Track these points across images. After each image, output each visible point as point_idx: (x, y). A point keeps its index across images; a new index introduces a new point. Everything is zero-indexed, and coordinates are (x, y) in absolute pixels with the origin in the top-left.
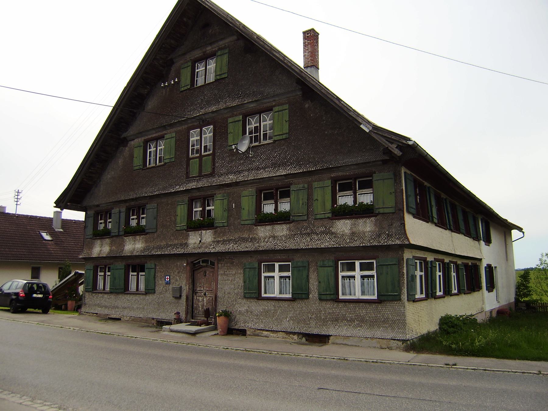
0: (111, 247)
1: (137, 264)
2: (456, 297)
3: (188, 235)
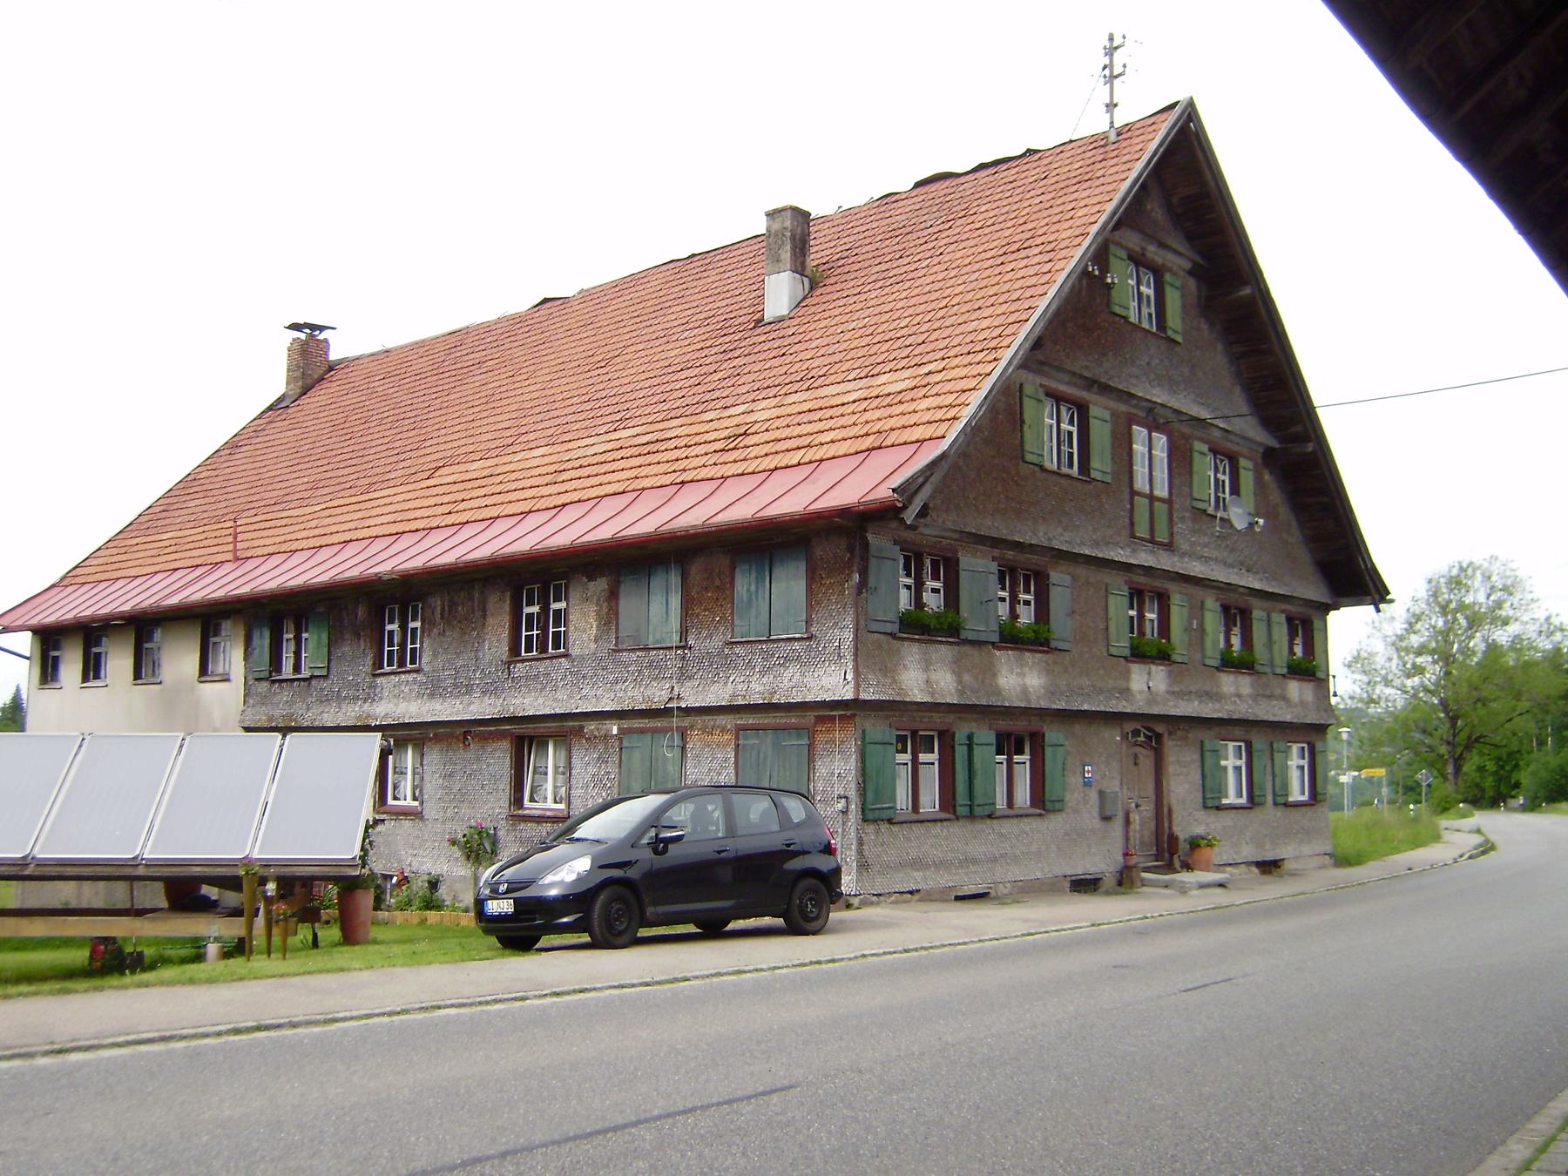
0: (958, 675)
1: (1020, 732)
2: (937, 829)
3: (1128, 672)
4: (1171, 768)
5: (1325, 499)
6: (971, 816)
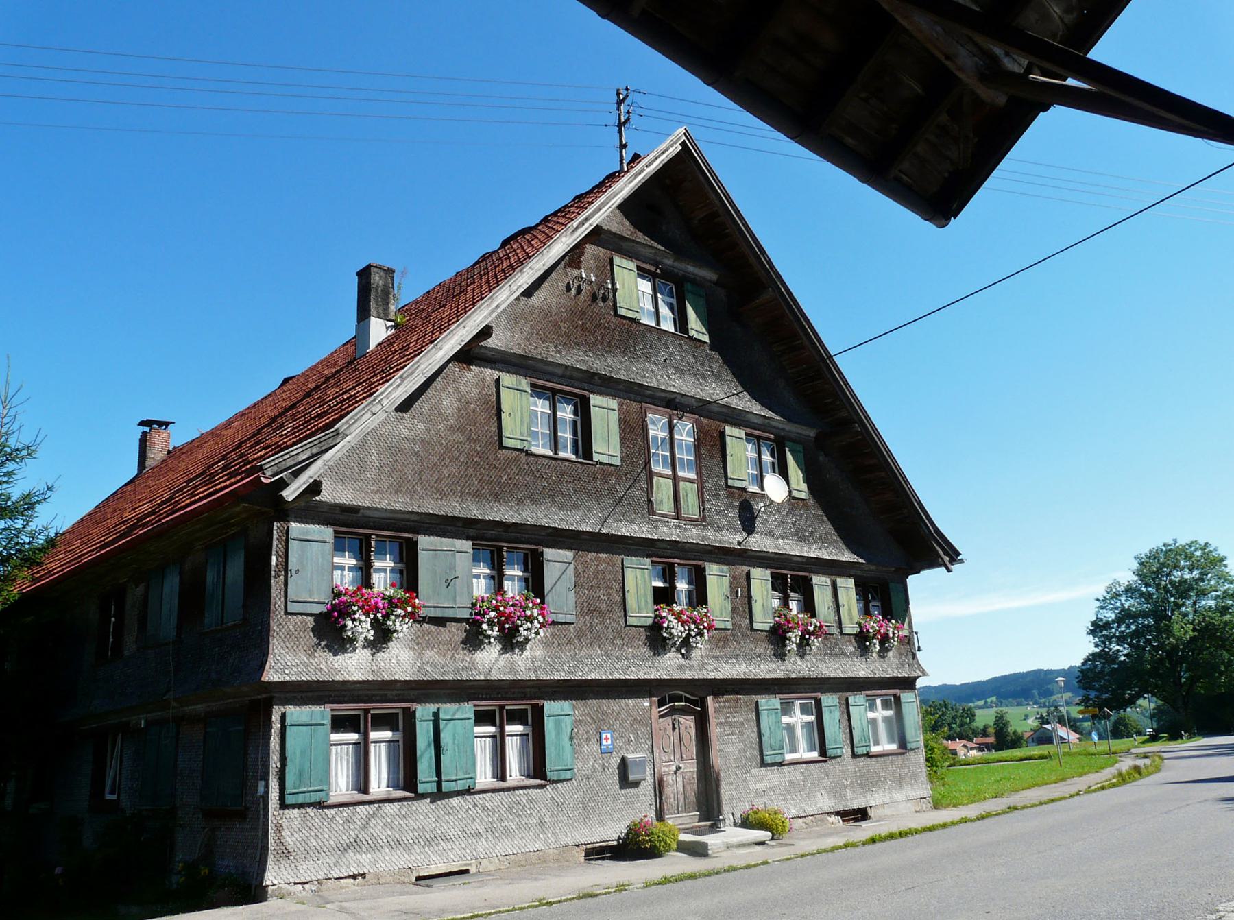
4: (715, 729)
5: (883, 474)
6: (439, 795)
